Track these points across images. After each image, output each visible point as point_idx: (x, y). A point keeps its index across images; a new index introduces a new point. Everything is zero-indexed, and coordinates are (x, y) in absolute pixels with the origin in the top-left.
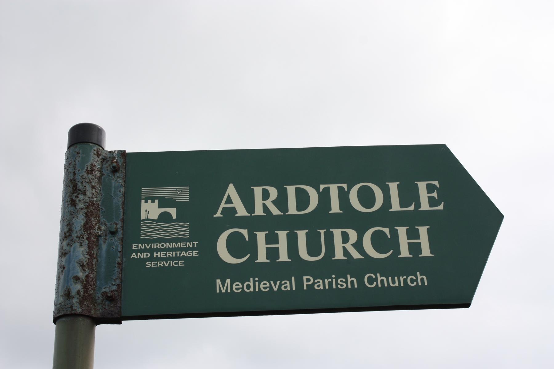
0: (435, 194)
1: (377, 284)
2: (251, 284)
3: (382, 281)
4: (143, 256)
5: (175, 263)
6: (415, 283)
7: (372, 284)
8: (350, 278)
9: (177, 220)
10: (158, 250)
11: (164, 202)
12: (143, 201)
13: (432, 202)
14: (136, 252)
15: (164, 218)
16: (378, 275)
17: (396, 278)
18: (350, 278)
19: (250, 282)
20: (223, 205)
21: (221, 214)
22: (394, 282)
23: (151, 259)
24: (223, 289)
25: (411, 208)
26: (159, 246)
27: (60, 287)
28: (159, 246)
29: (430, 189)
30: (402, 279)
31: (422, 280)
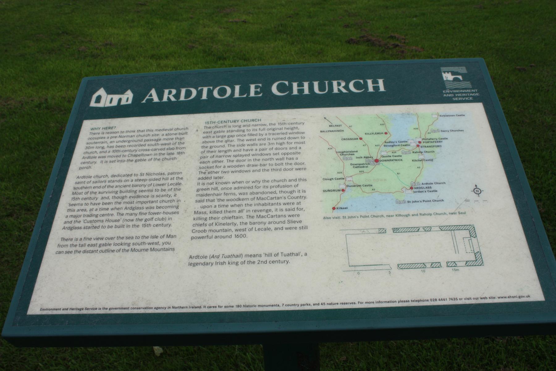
0: (259, 90)
4: (450, 95)
5: (468, 98)
9: (463, 81)
10: (457, 93)
11: (453, 73)
12: (443, 73)
13: (256, 93)
14: (446, 94)
15: (455, 80)
20: (147, 97)
21: (145, 101)
23: (455, 97)
25: (245, 96)
26: (457, 91)
28: (457, 91)
29: (256, 87)
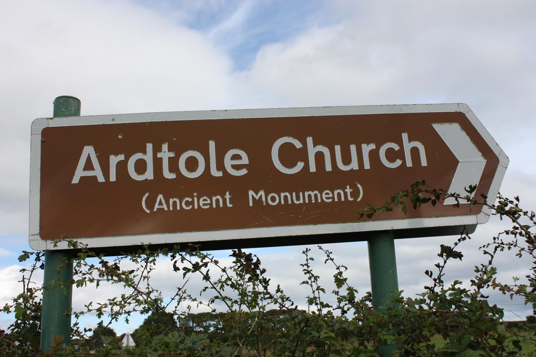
1: (307, 166)
2: (149, 158)
3: (319, 156)
6: (300, 166)
7: (290, 164)
8: (315, 145)
16: (310, 140)
17: (353, 148)
18: (315, 145)
19: (145, 152)
22: (347, 160)
24: (252, 195)
27: (358, 221)
30: (366, 149)
31: (415, 152)
